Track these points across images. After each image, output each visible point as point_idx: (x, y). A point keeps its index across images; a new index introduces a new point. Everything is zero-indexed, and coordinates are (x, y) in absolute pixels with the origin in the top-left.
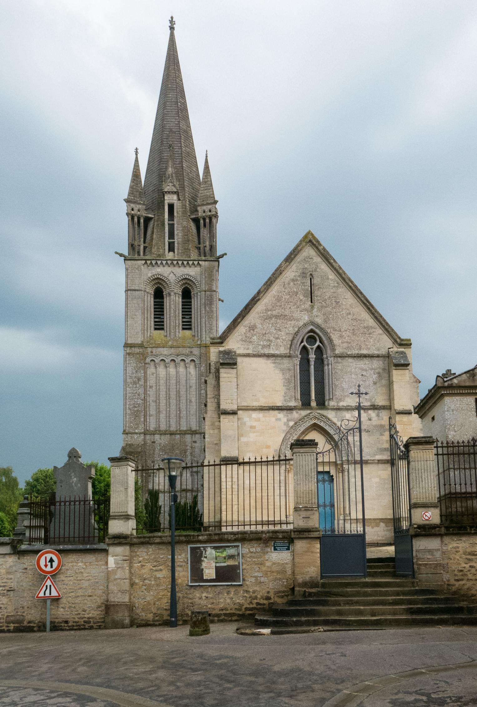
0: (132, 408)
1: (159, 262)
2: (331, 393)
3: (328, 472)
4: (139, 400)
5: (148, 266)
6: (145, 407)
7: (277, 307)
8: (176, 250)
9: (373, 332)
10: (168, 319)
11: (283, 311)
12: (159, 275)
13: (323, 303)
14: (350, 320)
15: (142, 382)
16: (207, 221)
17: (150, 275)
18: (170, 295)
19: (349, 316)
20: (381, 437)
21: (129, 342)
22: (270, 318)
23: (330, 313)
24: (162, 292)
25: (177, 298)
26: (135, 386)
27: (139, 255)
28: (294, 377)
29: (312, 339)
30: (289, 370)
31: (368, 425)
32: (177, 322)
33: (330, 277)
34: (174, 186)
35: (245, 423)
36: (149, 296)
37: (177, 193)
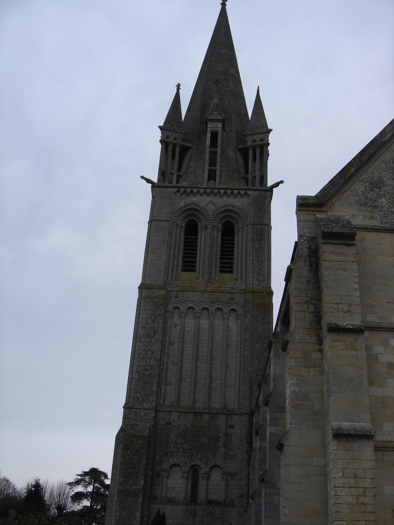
1: (195, 190)
6: (160, 371)
8: (217, 179)
10: (202, 257)
12: (194, 204)
15: (159, 336)
16: (258, 151)
17: (182, 204)
18: (206, 227)
24: (197, 225)
25: (215, 232)
26: (148, 340)
32: (214, 261)
36: (179, 229)
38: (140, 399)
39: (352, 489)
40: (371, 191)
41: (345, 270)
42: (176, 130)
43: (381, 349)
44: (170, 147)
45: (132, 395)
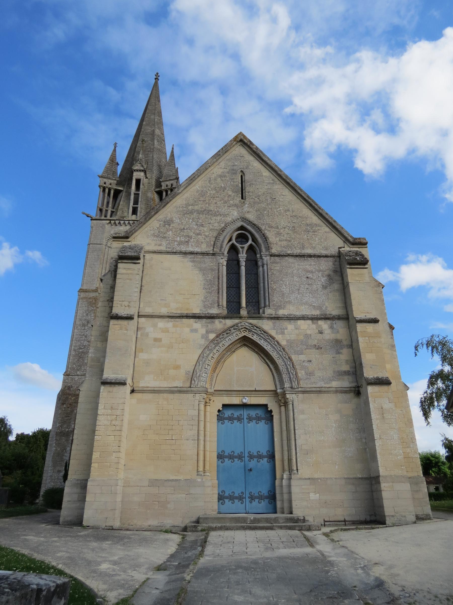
0: (78, 349)
1: (122, 222)
2: (267, 298)
3: (266, 406)
4: (85, 342)
5: (112, 225)
7: (200, 202)
8: (138, 213)
9: (318, 230)
11: (207, 205)
13: (256, 199)
14: (289, 216)
19: (288, 213)
20: (337, 355)
21: (85, 288)
22: (191, 212)
23: (265, 209)
26: (83, 328)
27: (105, 216)
28: (218, 279)
29: (242, 238)
30: (212, 270)
31: (318, 340)
33: (264, 174)
34: (142, 166)
35: (147, 335)
37: (145, 171)
38: (76, 369)
39: (109, 416)
40: (163, 227)
41: (131, 279)
42: (111, 178)
43: (152, 329)
44: (107, 190)
45: (70, 366)
